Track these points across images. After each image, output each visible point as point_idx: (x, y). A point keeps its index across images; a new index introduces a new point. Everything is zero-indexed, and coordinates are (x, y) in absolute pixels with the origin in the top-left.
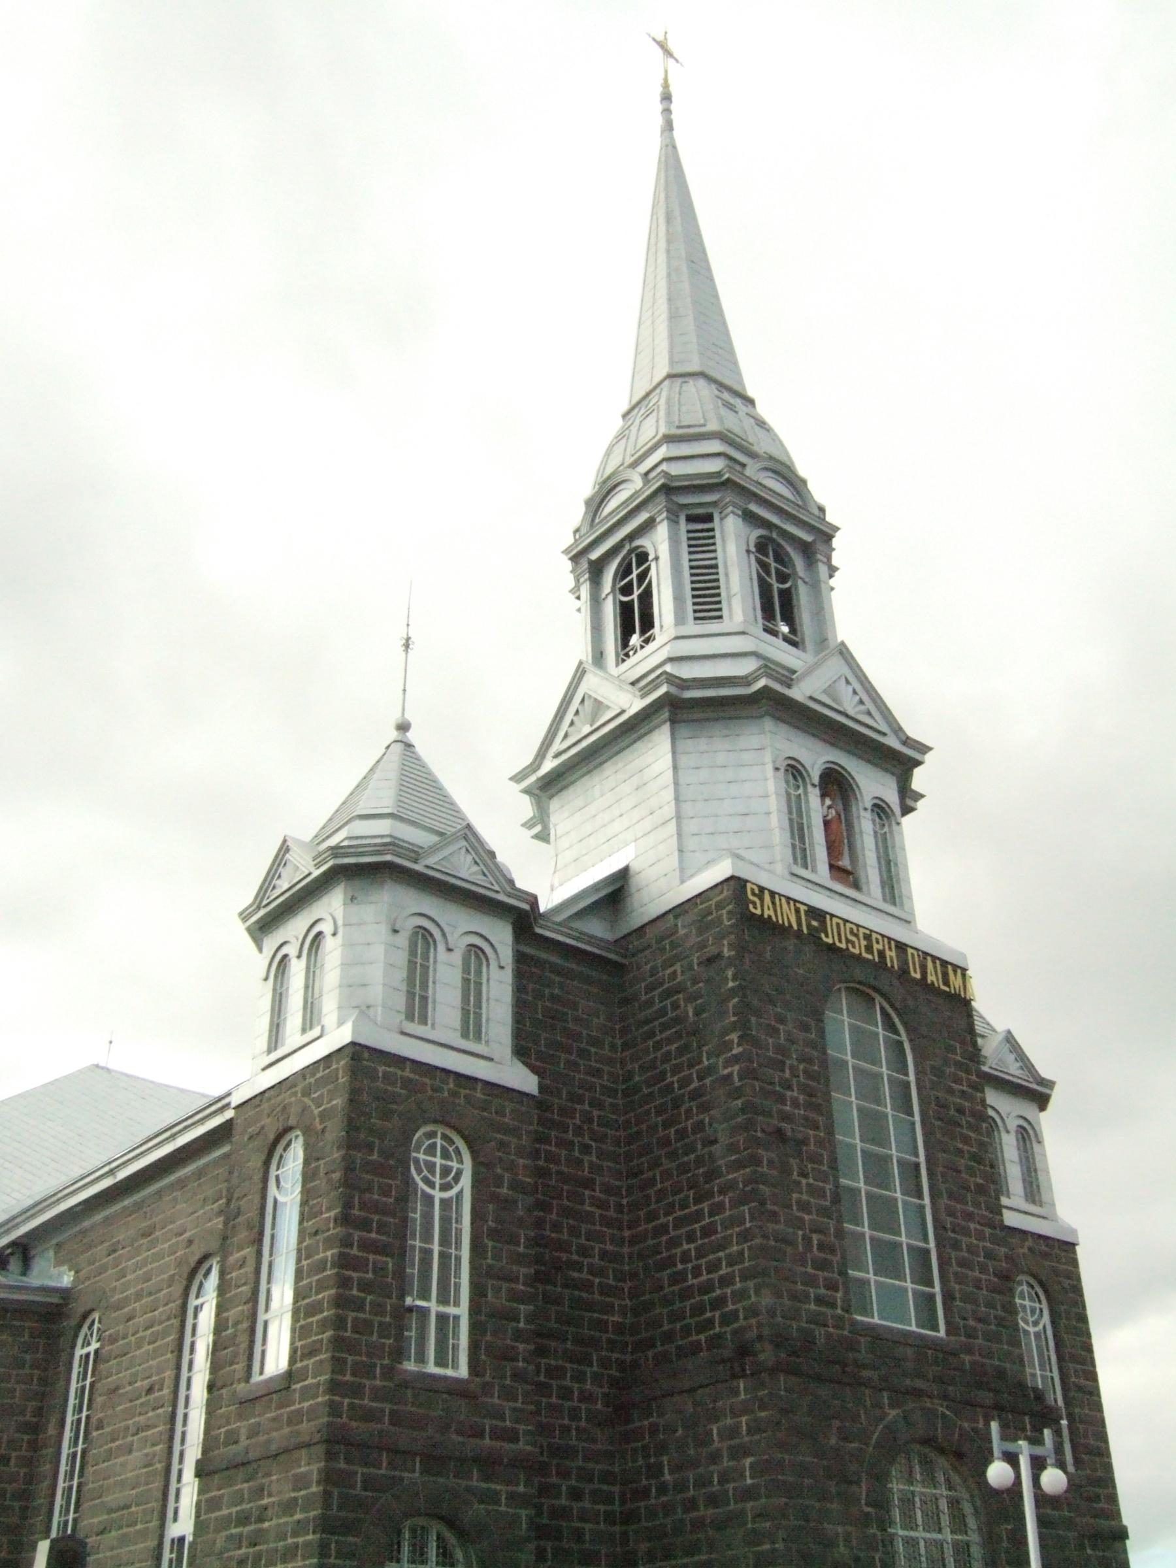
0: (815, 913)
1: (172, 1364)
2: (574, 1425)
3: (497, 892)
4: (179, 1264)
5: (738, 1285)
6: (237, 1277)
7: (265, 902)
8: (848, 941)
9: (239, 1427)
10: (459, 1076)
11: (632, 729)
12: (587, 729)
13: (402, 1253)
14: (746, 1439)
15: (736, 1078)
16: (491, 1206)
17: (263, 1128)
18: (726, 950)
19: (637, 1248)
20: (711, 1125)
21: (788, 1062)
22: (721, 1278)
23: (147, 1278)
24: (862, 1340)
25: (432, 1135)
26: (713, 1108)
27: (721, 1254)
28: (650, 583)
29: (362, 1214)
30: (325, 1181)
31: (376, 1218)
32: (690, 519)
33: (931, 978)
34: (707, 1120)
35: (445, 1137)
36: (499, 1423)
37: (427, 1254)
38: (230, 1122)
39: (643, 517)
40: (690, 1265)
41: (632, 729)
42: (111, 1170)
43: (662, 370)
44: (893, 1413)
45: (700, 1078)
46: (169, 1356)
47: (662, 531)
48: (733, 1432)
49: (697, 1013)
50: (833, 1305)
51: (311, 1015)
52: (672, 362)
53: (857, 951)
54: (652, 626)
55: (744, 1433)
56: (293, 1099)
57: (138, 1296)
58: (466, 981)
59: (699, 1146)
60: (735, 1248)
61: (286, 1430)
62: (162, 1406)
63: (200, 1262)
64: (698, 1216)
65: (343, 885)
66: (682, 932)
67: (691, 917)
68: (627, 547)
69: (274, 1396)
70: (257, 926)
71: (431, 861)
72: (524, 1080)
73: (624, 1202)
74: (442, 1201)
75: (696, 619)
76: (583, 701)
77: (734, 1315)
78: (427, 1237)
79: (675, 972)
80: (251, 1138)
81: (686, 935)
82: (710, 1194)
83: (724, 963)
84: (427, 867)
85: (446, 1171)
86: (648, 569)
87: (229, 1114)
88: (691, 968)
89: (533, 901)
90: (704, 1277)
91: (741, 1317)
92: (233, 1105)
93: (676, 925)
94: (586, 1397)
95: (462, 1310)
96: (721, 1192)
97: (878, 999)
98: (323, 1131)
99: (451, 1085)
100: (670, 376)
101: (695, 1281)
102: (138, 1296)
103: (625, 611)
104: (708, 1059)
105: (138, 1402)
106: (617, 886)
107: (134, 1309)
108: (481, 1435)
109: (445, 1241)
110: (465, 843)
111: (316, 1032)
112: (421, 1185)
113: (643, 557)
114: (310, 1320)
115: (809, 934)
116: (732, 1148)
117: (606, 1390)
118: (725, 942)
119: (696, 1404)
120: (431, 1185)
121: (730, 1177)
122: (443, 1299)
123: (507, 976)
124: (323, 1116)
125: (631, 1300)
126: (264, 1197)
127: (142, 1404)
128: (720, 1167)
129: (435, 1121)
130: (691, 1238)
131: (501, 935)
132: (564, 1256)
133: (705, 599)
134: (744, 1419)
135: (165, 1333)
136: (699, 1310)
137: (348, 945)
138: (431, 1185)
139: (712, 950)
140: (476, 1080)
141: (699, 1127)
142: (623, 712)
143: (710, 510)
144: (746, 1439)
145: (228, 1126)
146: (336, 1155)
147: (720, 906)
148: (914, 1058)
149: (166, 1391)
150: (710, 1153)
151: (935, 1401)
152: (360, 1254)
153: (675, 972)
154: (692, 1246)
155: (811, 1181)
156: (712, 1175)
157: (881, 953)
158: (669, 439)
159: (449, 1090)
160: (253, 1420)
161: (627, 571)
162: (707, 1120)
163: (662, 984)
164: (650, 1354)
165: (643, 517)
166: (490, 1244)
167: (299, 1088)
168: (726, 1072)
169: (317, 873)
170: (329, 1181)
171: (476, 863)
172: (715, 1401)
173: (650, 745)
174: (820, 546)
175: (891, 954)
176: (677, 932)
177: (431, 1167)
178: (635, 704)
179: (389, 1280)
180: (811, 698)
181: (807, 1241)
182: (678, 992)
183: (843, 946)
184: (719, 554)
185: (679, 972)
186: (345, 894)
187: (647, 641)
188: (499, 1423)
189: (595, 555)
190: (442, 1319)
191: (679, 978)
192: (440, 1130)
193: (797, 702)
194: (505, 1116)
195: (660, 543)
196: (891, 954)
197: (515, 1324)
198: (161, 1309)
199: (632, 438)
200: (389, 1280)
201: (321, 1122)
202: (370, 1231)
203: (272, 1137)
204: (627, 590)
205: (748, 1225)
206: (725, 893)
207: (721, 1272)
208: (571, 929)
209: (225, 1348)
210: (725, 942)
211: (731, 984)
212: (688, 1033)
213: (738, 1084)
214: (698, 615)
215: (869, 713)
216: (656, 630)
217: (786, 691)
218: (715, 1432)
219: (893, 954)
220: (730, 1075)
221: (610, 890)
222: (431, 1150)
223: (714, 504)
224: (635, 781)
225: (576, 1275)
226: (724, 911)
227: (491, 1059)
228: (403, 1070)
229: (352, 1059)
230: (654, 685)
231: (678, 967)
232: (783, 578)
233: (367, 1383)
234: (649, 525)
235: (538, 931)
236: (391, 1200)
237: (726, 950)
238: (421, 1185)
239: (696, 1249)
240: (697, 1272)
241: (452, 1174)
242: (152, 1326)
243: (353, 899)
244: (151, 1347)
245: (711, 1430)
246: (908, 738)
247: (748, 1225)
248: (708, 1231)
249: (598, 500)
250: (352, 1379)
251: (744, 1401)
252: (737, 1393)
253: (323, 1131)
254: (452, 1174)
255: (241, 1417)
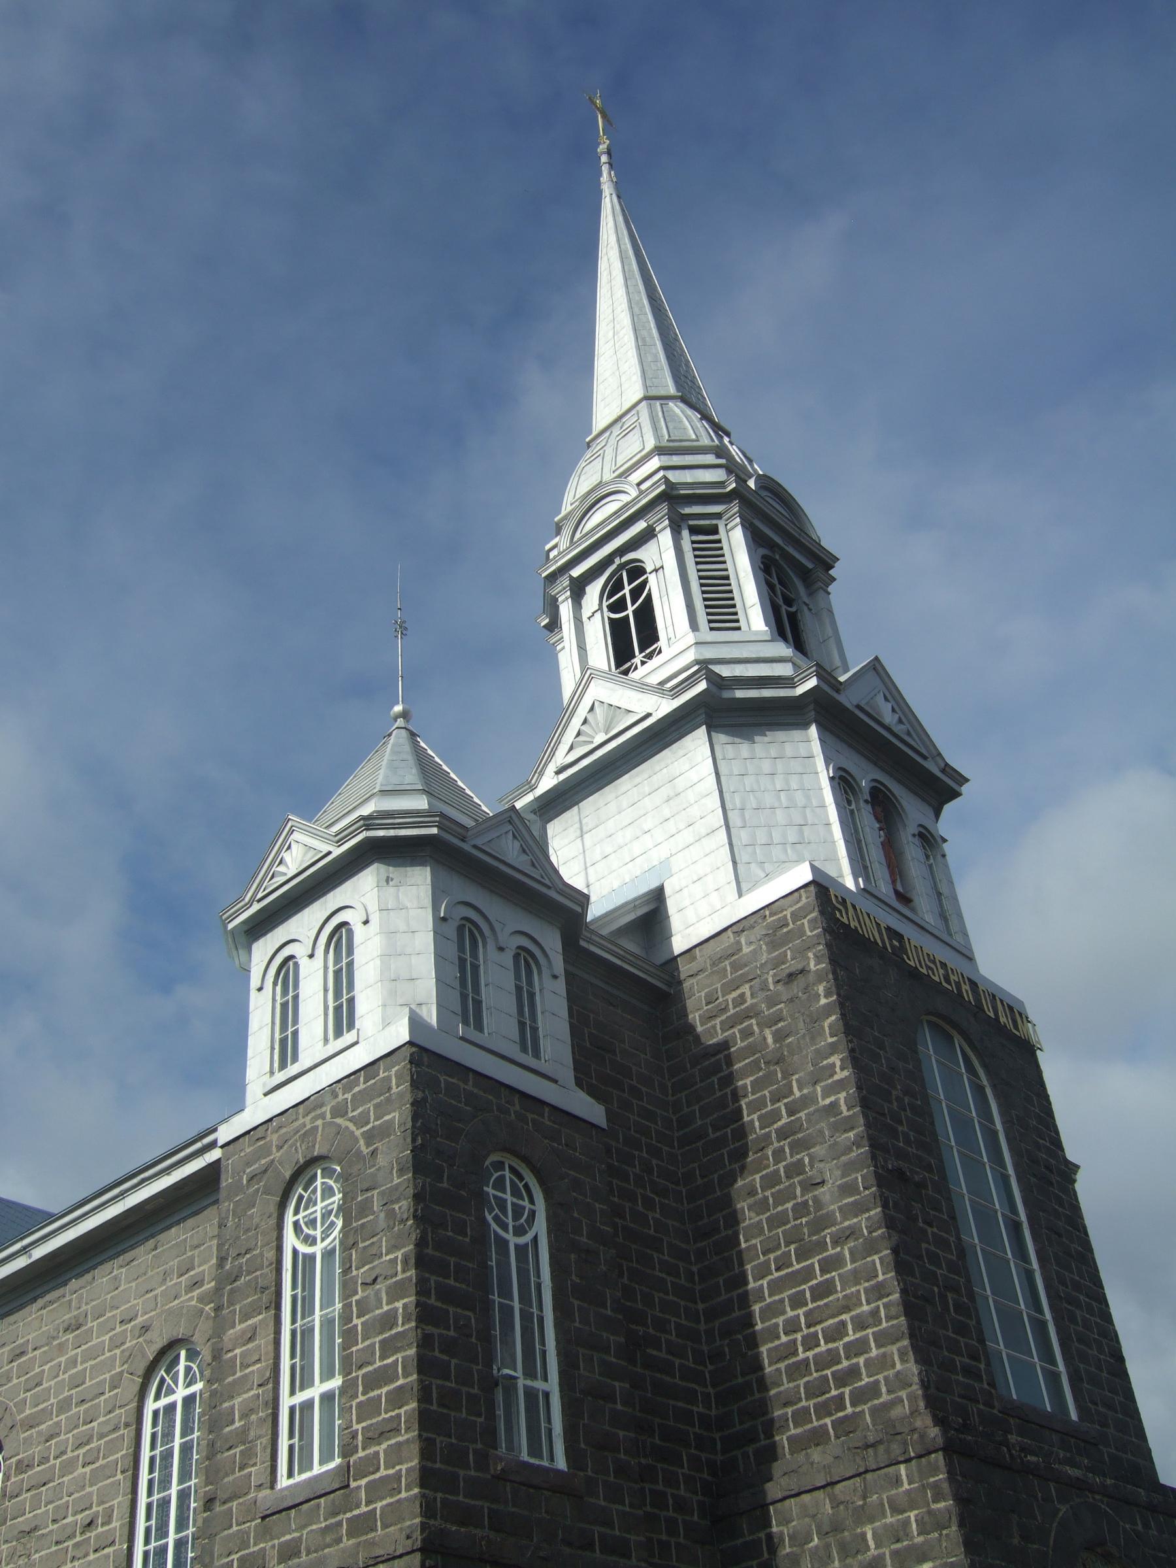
0: (893, 933)
1: (126, 1486)
2: (673, 1541)
3: (549, 888)
4: (128, 1358)
5: (874, 1352)
6: (243, 1355)
7: (260, 895)
8: (928, 968)
9: (264, 1549)
10: (524, 1095)
11: (658, 737)
12: (600, 738)
13: (487, 1306)
14: (919, 1540)
15: (844, 1108)
16: (573, 1256)
17: (273, 1161)
18: (812, 964)
19: (717, 1324)
20: (812, 1167)
21: (894, 1093)
22: (847, 1346)
23: (77, 1382)
24: (1012, 1421)
25: (499, 1166)
26: (814, 1145)
27: (845, 1317)
28: (649, 596)
29: (437, 1254)
30: (382, 1215)
31: (452, 1260)
32: (694, 530)
33: (1003, 1020)
34: (807, 1160)
35: (513, 1170)
36: (608, 1531)
37: (507, 1311)
38: (215, 1166)
39: (641, 525)
40: (799, 1336)
41: (658, 737)
42: (25, 1248)
43: (639, 395)
44: (1063, 1509)
45: (791, 1113)
46: (119, 1476)
47: (665, 538)
48: (899, 1533)
49: (779, 1037)
50: (979, 1378)
51: (343, 1017)
52: (646, 387)
53: (936, 979)
54: (656, 639)
55: (915, 1533)
56: (319, 1122)
57: (64, 1406)
58: (519, 989)
59: (798, 1191)
60: (866, 1308)
61: (347, 1543)
62: (113, 1543)
63: (162, 1353)
64: (808, 1274)
65: (375, 866)
66: (746, 950)
67: (759, 931)
68: (617, 561)
69: (322, 1500)
70: (246, 928)
71: (479, 842)
72: (592, 1110)
73: (695, 1269)
74: (517, 1246)
75: (711, 629)
76: (592, 709)
77: (873, 1391)
78: (506, 1293)
79: (742, 995)
80: (251, 1179)
81: (754, 952)
82: (822, 1246)
83: (811, 978)
84: (475, 847)
85: (518, 1211)
86: (645, 582)
87: (215, 1154)
88: (764, 987)
89: (583, 900)
90: (823, 1347)
91: (884, 1389)
92: (220, 1143)
93: (739, 943)
94: (681, 1506)
95: (553, 1385)
96: (836, 1243)
97: (958, 1040)
98: (374, 1153)
99: (517, 1107)
100: (646, 398)
101: (810, 1354)
102: (64, 1406)
103: (618, 631)
104: (800, 1089)
105: (70, 1543)
106: (652, 907)
107: (58, 1424)
108: (590, 1546)
109: (525, 1298)
110: (510, 827)
111: (348, 1038)
112: (494, 1226)
113: (637, 571)
114: (376, 1393)
115: (893, 953)
116: (847, 1189)
117: (700, 1497)
118: (811, 955)
119: (836, 1503)
120: (504, 1227)
121: (847, 1223)
122: (530, 1373)
123: (561, 986)
124: (370, 1137)
125: (714, 1386)
126: (279, 1249)
127: (76, 1545)
128: (833, 1212)
129: (505, 1149)
130: (797, 1301)
131: (552, 941)
132: (641, 1330)
133: (718, 607)
134: (912, 1515)
135: (112, 1448)
136: (819, 1388)
137: (389, 934)
138: (504, 1227)
139: (792, 965)
140: (543, 1103)
141: (796, 1169)
142: (649, 715)
143: (714, 522)
144: (920, 1539)
145: (212, 1173)
146: (396, 1181)
147: (796, 916)
148: (1000, 1106)
149: (115, 1524)
150: (816, 1200)
151: (1097, 1497)
152: (439, 1304)
153: (742, 995)
154: (801, 1311)
155: (935, 1230)
156: (819, 1225)
157: (958, 984)
158: (660, 450)
159: (515, 1112)
160: (288, 1537)
161: (618, 586)
162: (807, 1160)
163: (725, 1010)
164: (750, 1450)
165: (641, 525)
166: (576, 1303)
167: (327, 1109)
168: (828, 1101)
169: (337, 852)
170: (391, 1214)
171: (524, 851)
172: (864, 1498)
173: (681, 753)
174: (820, 573)
175: (965, 987)
176: (740, 950)
177: (502, 1204)
178: (663, 707)
179: (473, 1340)
180: (858, 707)
181: (943, 1297)
182: (749, 1017)
183: (924, 971)
184: (729, 565)
185: (748, 994)
186: (378, 874)
187: (650, 656)
188: (608, 1531)
189: (576, 572)
190: (531, 1394)
191: (749, 1001)
192: (509, 1160)
193: (845, 709)
194: (575, 1150)
195: (661, 555)
196: (965, 987)
197: (611, 1406)
198: (102, 1419)
199: (608, 458)
200: (473, 1340)
201: (368, 1145)
202: (448, 1277)
203: (288, 1174)
204: (619, 606)
205: (881, 1278)
206: (804, 900)
207: (846, 1339)
208: (617, 945)
209: (230, 1448)
210: (811, 955)
211: (823, 1001)
212: (767, 1063)
213: (845, 1113)
214: (713, 625)
215: (909, 734)
216: (662, 643)
217: (835, 695)
218: (869, 1536)
219: (968, 988)
220: (834, 1105)
221: (640, 912)
222: (500, 1184)
223: (718, 516)
224: (665, 791)
225: (655, 1353)
226: (805, 921)
227: (556, 1082)
228: (466, 1082)
229: (411, 1062)
230: (689, 682)
231: (746, 989)
232: (789, 602)
233: (462, 1473)
234: (648, 535)
235: (583, 943)
236: (468, 1240)
237: (812, 964)
238: (494, 1226)
239: (806, 1314)
240: (811, 1342)
241: (525, 1216)
242: (88, 1442)
243: (388, 880)
244: (88, 1469)
245: (864, 1535)
246: (947, 764)
247: (881, 1278)
248: (825, 1290)
249: (578, 514)
250: (443, 1467)
251: (908, 1492)
252: (898, 1482)
253: (374, 1153)
254: (525, 1216)
255: (265, 1533)
